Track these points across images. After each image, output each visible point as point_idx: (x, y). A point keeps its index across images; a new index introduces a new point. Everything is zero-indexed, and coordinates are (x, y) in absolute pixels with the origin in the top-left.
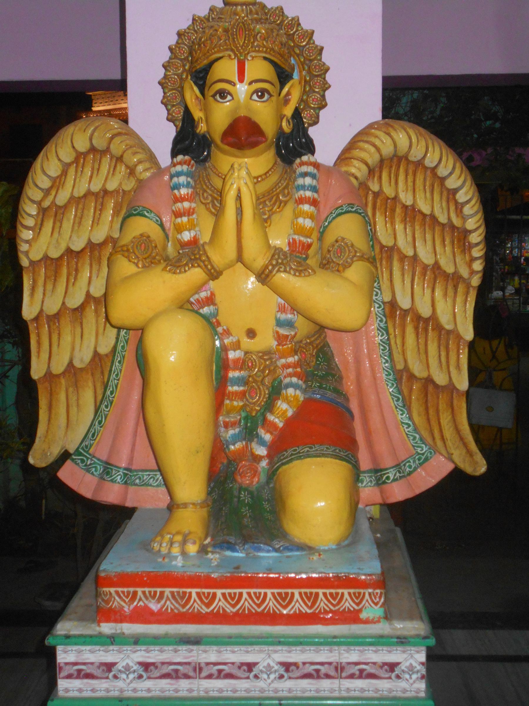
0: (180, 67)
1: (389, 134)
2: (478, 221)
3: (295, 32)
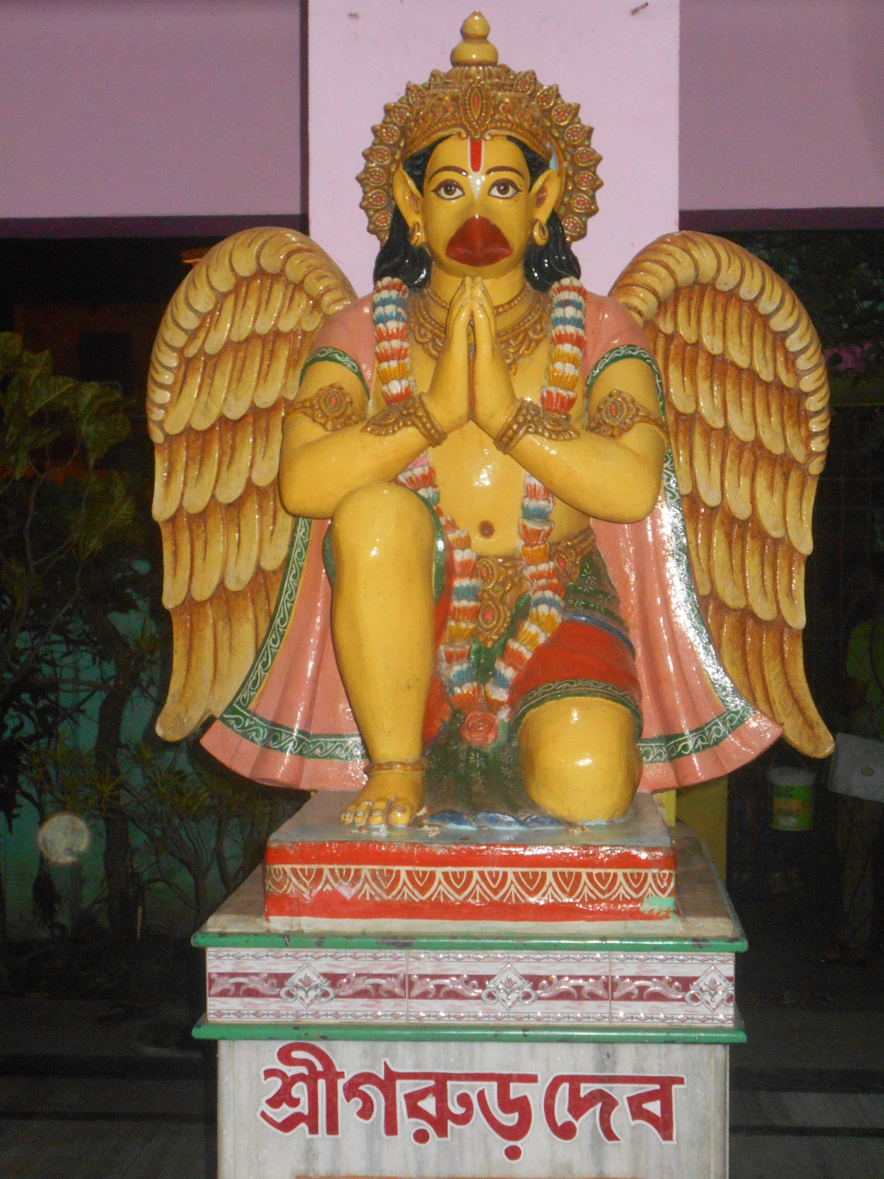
0: (388, 155)
1: (687, 251)
2: (818, 380)
3: (553, 107)
